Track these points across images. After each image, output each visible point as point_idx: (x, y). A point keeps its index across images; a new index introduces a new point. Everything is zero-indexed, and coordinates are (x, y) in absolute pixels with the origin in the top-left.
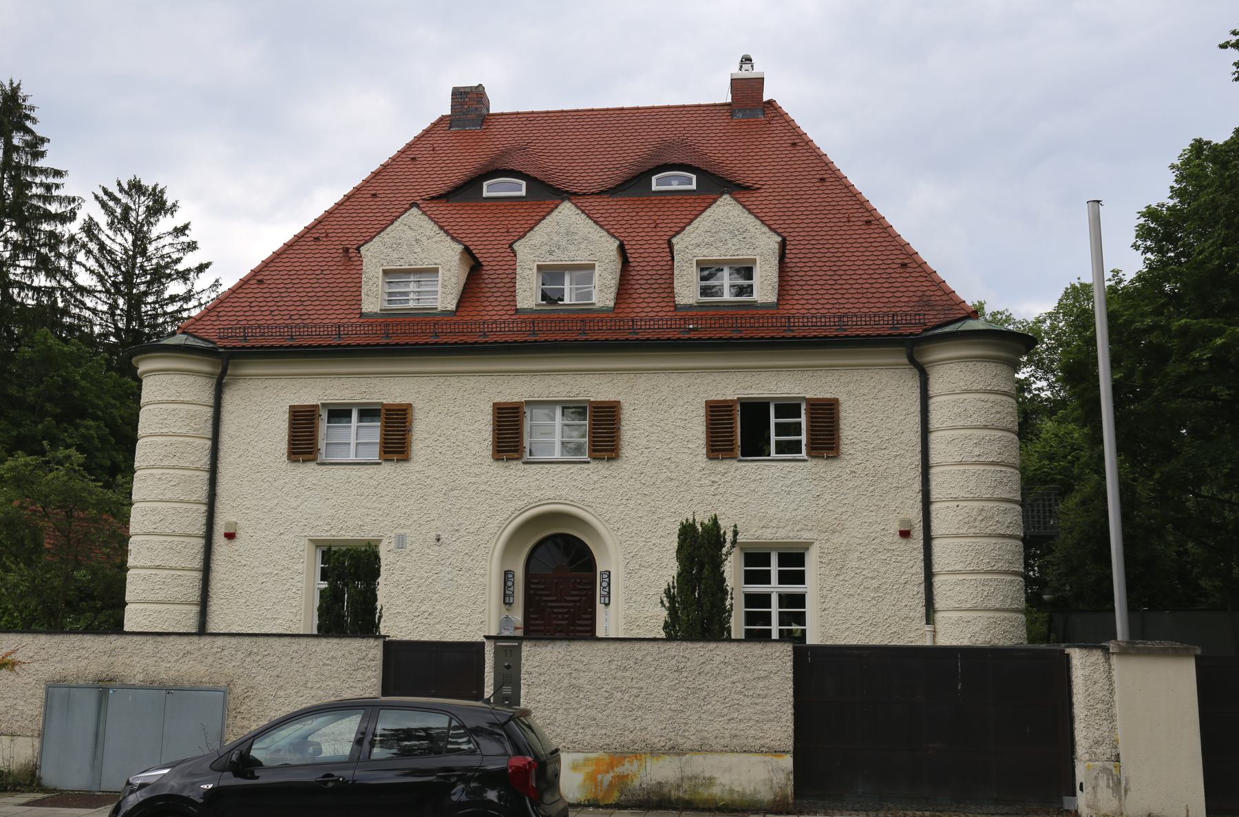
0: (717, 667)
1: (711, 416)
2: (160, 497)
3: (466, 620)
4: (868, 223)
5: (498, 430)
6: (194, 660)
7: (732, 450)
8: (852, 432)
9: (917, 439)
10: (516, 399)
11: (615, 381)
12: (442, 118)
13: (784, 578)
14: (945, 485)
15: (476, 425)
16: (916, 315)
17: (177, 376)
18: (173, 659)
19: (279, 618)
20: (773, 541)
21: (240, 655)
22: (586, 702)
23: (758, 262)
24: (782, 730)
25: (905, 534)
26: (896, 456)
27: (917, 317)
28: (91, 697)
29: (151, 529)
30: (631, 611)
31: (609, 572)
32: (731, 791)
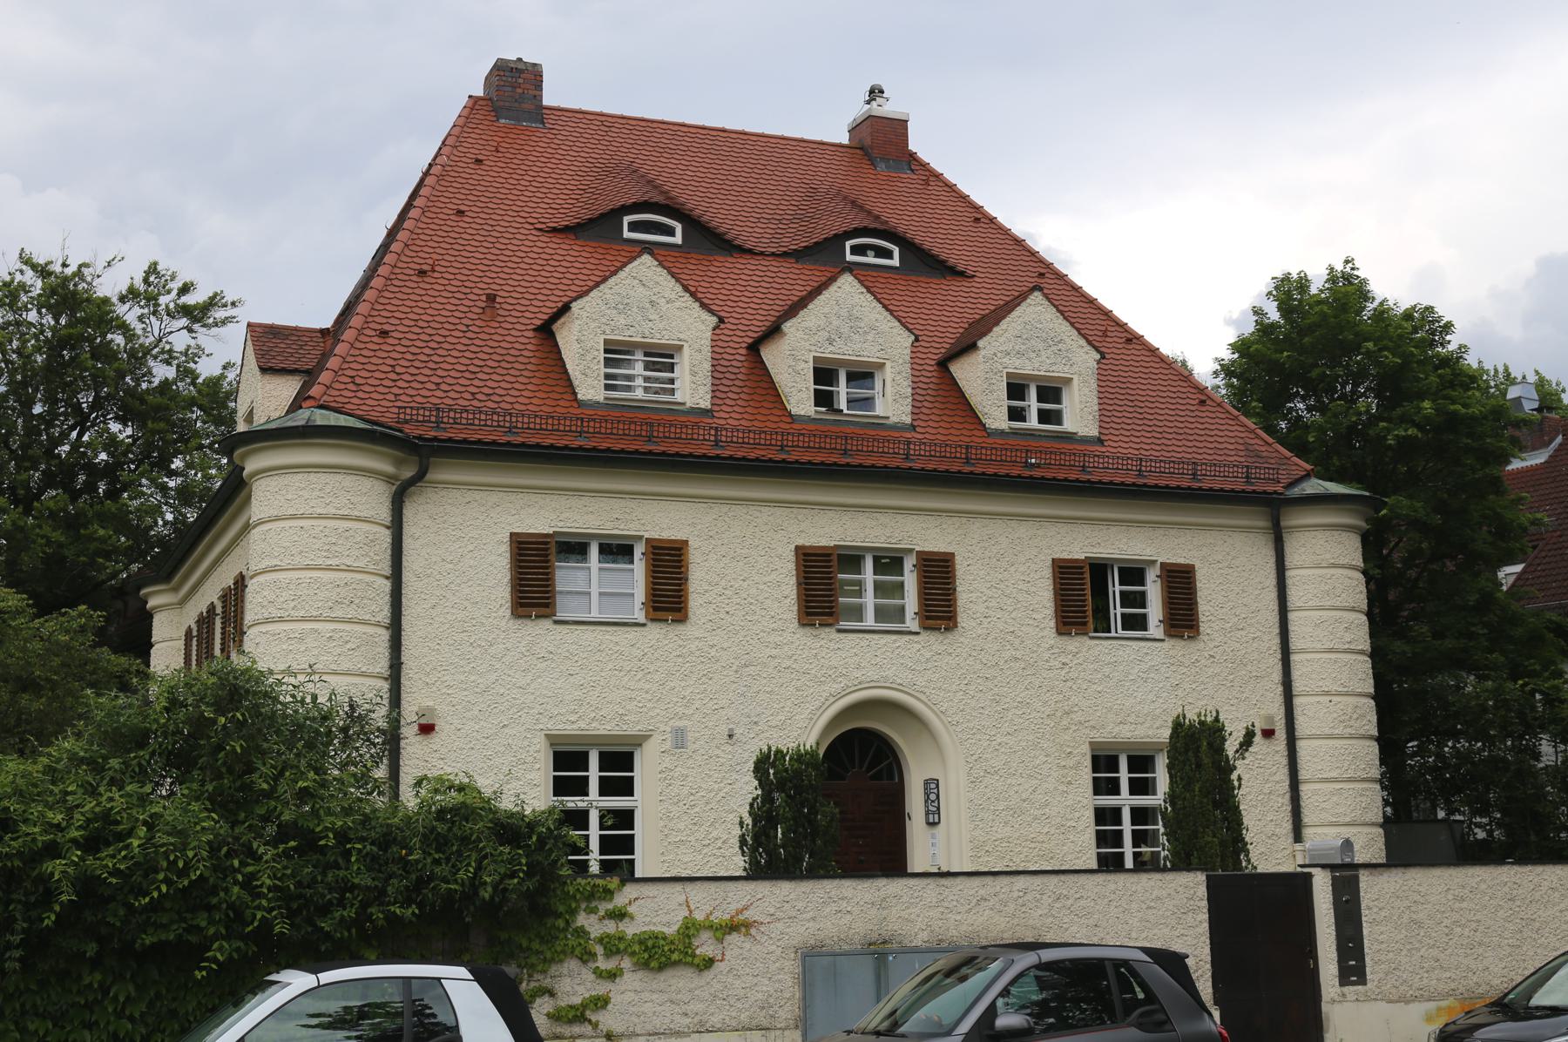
2: (334, 667)
7: (1085, 624)
9: (1274, 618)
11: (944, 526)
14: (1314, 676)
15: (774, 576)
17: (349, 478)
18: (963, 909)
20: (1132, 740)
23: (1075, 382)
26: (1254, 639)
28: (866, 968)
30: (977, 833)
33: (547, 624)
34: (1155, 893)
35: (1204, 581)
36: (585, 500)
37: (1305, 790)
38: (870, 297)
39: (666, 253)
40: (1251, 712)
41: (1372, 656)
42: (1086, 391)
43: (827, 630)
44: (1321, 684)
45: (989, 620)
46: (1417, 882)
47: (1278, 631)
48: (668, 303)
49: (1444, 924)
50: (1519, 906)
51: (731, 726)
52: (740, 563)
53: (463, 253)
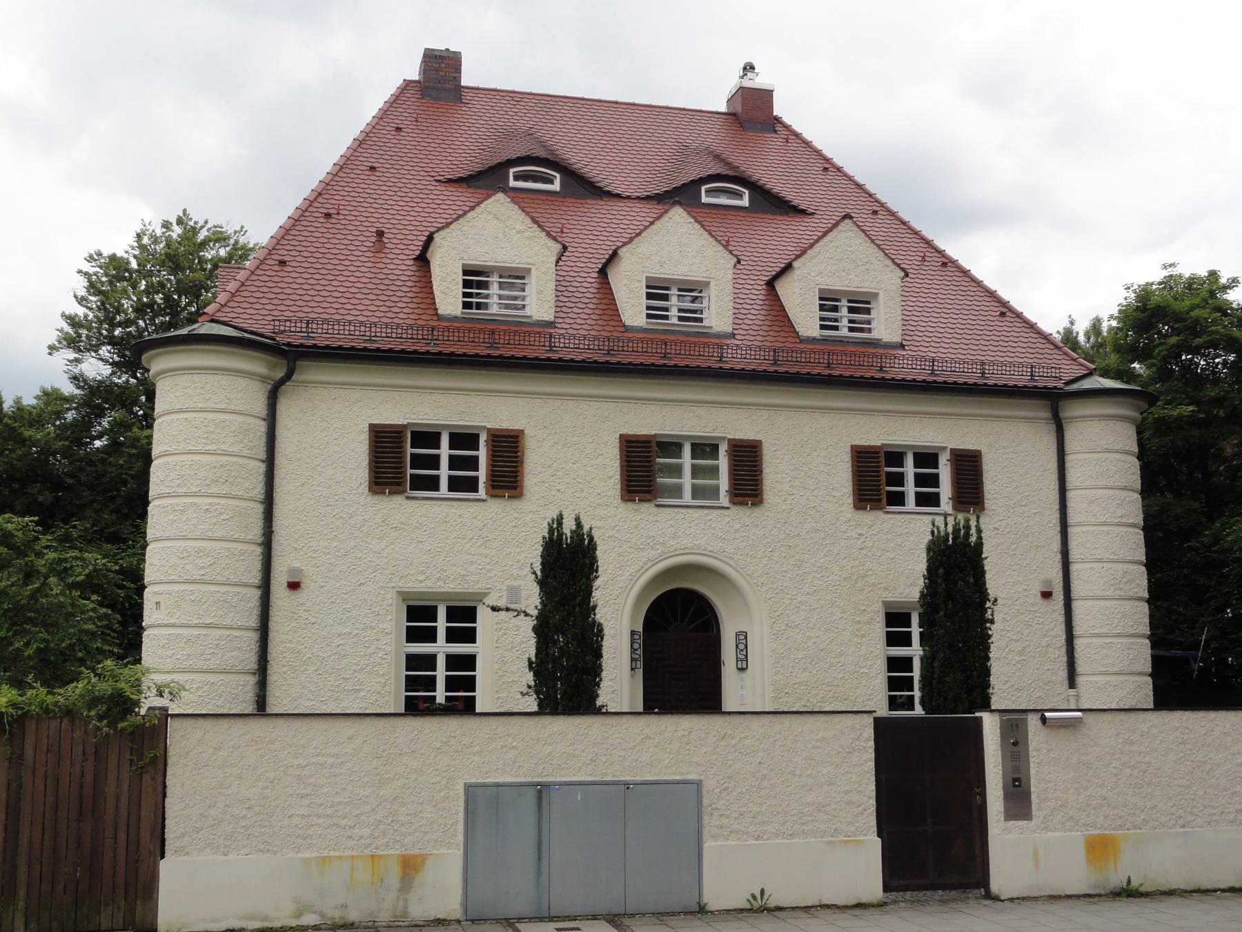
0: (1218, 738)
2: (209, 534)
4: (944, 264)
6: (656, 746)
7: (880, 500)
11: (754, 418)
12: (408, 84)
13: (453, 636)
14: (1088, 546)
15: (600, 459)
16: (286, 321)
17: (226, 378)
19: (363, 690)
25: (1047, 595)
26: (1035, 514)
27: (288, 324)
28: (530, 799)
31: (746, 633)
34: (821, 734)
37: (1079, 644)
38: (697, 226)
39: (736, 214)
40: (1032, 577)
41: (1144, 529)
43: (647, 505)
44: (1094, 552)
45: (792, 497)
47: (1058, 507)
48: (518, 233)
49: (1114, 765)
50: (1190, 750)
53: (614, 221)
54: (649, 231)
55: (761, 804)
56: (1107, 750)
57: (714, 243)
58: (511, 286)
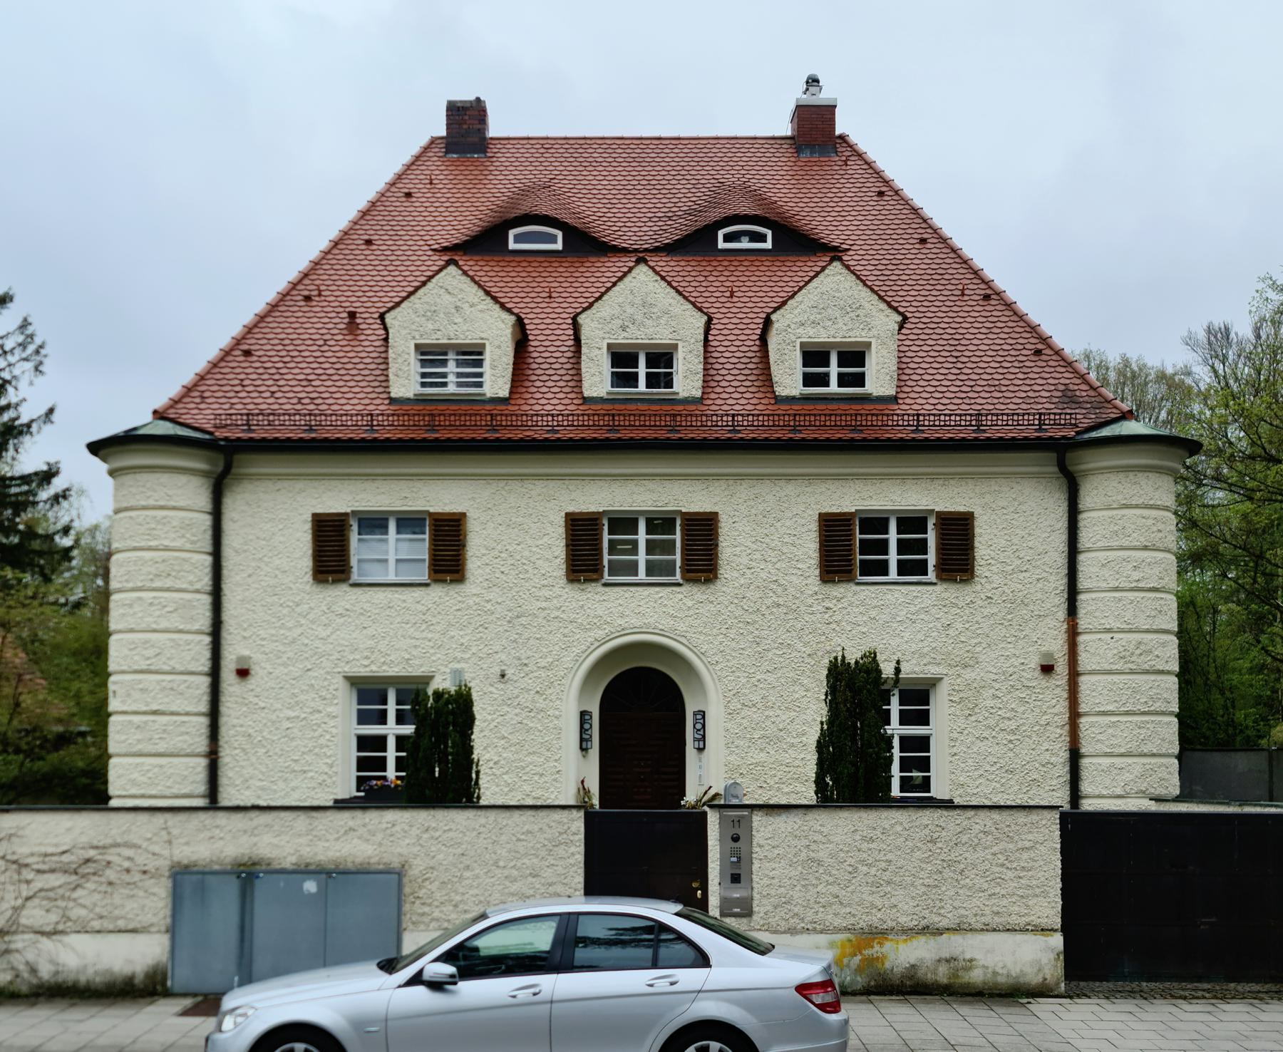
1: (826, 531)
2: (154, 626)
3: (539, 770)
5: (573, 545)
7: (850, 571)
8: (989, 551)
10: (593, 509)
11: (711, 489)
12: (433, 141)
15: (545, 539)
21: (415, 831)
22: (827, 878)
23: (873, 346)
24: (1049, 908)
28: (231, 888)
29: (143, 665)
30: (731, 758)
32: (995, 973)
33: (344, 588)
34: (526, 827)
35: (985, 527)
36: (378, 483)
42: (885, 352)
44: (1103, 621)
46: (820, 823)
48: (471, 306)
50: (941, 848)
51: (503, 668)
52: (516, 530)
54: (611, 293)
55: (463, 894)
56: (841, 847)
57: (682, 301)
58: (432, 363)
